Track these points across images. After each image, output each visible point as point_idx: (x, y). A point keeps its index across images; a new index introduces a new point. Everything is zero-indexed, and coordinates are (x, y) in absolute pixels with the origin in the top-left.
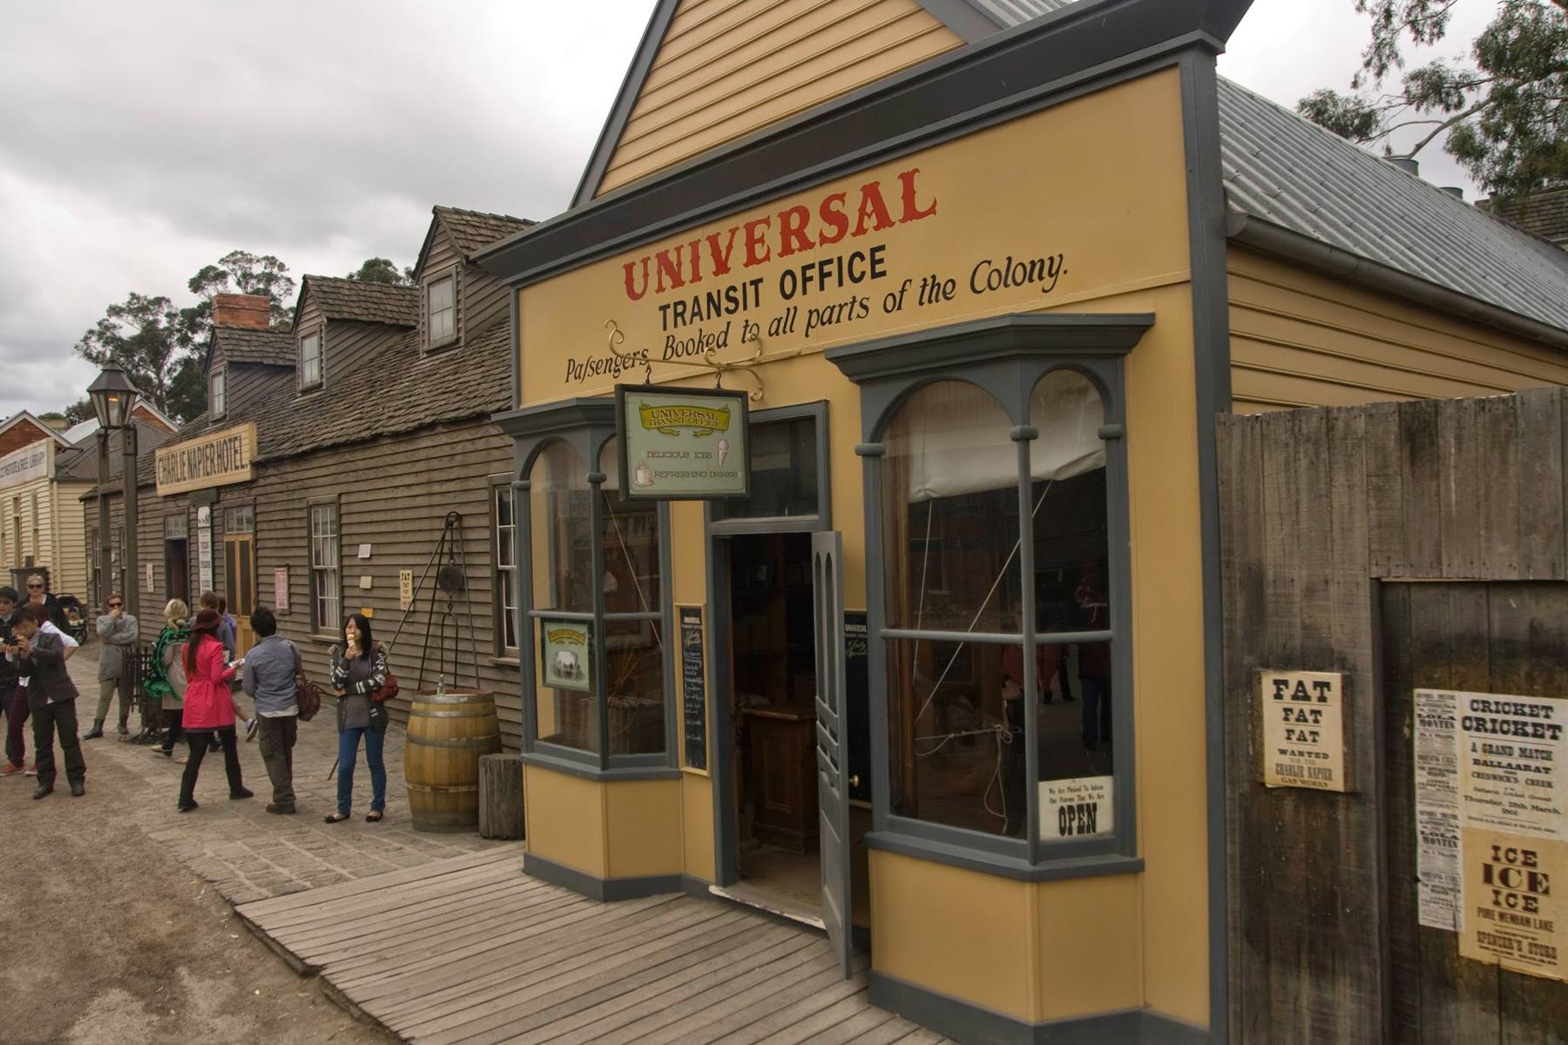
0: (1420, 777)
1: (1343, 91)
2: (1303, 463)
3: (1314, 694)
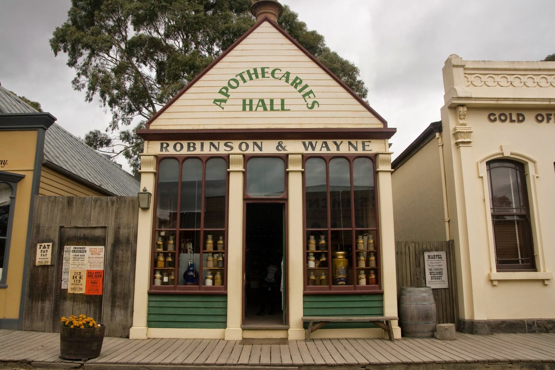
0: (64, 262)
1: (103, 132)
2: (50, 205)
3: (47, 247)
